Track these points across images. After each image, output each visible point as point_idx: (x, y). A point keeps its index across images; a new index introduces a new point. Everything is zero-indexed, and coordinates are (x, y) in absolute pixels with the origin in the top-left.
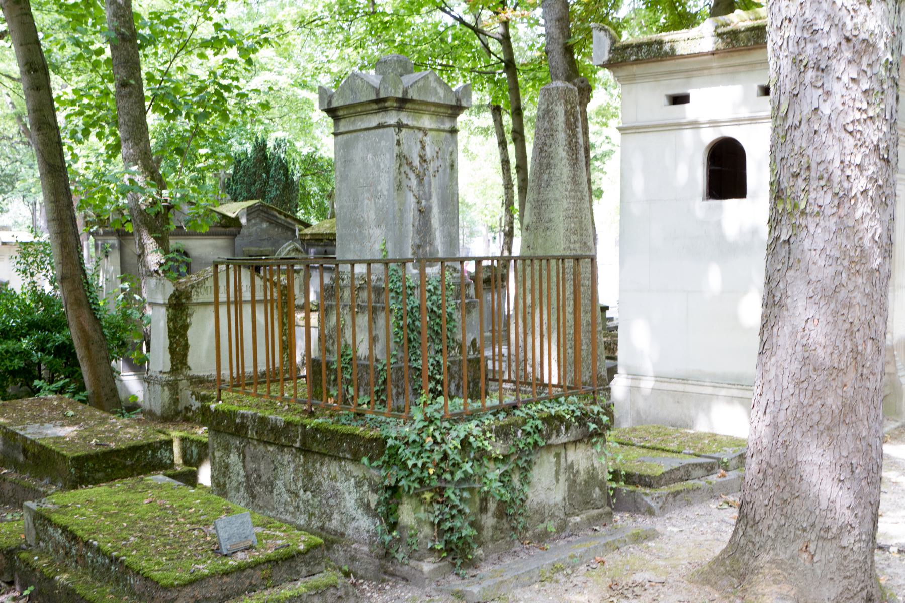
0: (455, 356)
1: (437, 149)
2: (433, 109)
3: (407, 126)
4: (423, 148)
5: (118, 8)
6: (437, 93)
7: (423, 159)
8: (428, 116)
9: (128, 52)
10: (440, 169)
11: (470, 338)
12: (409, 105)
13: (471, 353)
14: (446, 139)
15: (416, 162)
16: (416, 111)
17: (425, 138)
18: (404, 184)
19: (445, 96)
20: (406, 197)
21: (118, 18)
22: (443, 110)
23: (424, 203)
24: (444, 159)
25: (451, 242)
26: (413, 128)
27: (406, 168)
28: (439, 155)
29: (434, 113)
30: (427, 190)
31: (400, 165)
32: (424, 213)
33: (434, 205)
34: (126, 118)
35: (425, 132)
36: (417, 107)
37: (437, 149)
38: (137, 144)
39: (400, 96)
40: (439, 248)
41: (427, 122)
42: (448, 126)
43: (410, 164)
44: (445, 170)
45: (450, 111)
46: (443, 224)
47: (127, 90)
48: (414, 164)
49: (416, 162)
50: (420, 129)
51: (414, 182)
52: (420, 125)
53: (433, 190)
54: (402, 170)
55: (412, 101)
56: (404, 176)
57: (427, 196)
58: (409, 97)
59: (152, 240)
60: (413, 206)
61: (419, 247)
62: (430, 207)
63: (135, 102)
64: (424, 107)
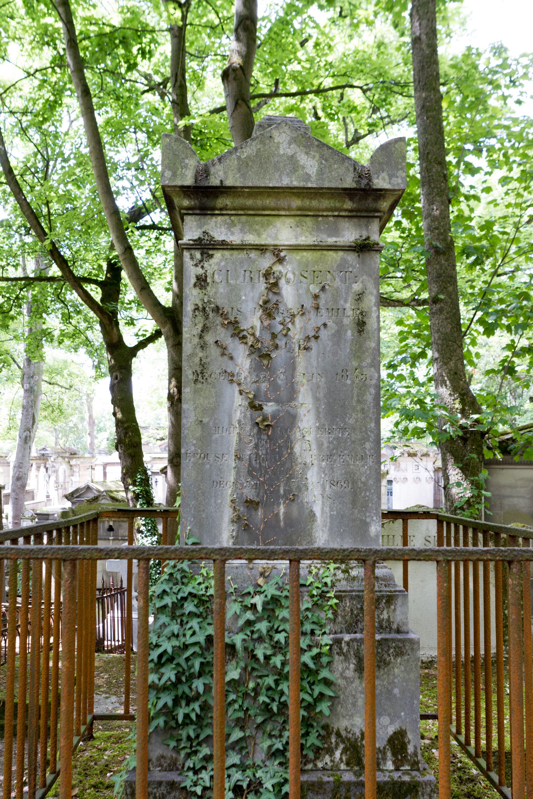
0: (335, 768)
1: (315, 289)
2: (296, 203)
3: (224, 246)
4: (274, 287)
5: (432, 221)
6: (293, 163)
7: (269, 309)
8: (290, 221)
9: (441, 265)
10: (324, 334)
11: (387, 728)
12: (221, 202)
13: (390, 765)
14: (342, 267)
15: (253, 320)
16: (256, 212)
17: (278, 268)
18: (215, 369)
19: (320, 172)
20: (219, 395)
21: (432, 231)
22: (326, 203)
23: (269, 408)
24: (337, 311)
25: (355, 494)
26: (241, 247)
27: (223, 335)
28: (322, 302)
29: (302, 214)
30: (281, 379)
31: (205, 329)
32: (271, 432)
33: (302, 411)
34: (436, 335)
35: (277, 253)
36: (249, 202)
37: (315, 289)
38: (445, 364)
39: (189, 181)
40: (317, 509)
41: (284, 232)
42: (350, 234)
43: (235, 328)
44: (339, 335)
45: (348, 205)
46: (330, 455)
47: (438, 306)
48: (244, 325)
49: (253, 320)
50: (262, 249)
51: (243, 361)
52: (265, 239)
53: (299, 378)
54: (210, 338)
55: (222, 190)
56: (214, 351)
57: (283, 394)
58: (214, 181)
59: (458, 470)
60: (238, 415)
61: (251, 504)
62: (292, 419)
63: (447, 319)
64: (269, 202)
